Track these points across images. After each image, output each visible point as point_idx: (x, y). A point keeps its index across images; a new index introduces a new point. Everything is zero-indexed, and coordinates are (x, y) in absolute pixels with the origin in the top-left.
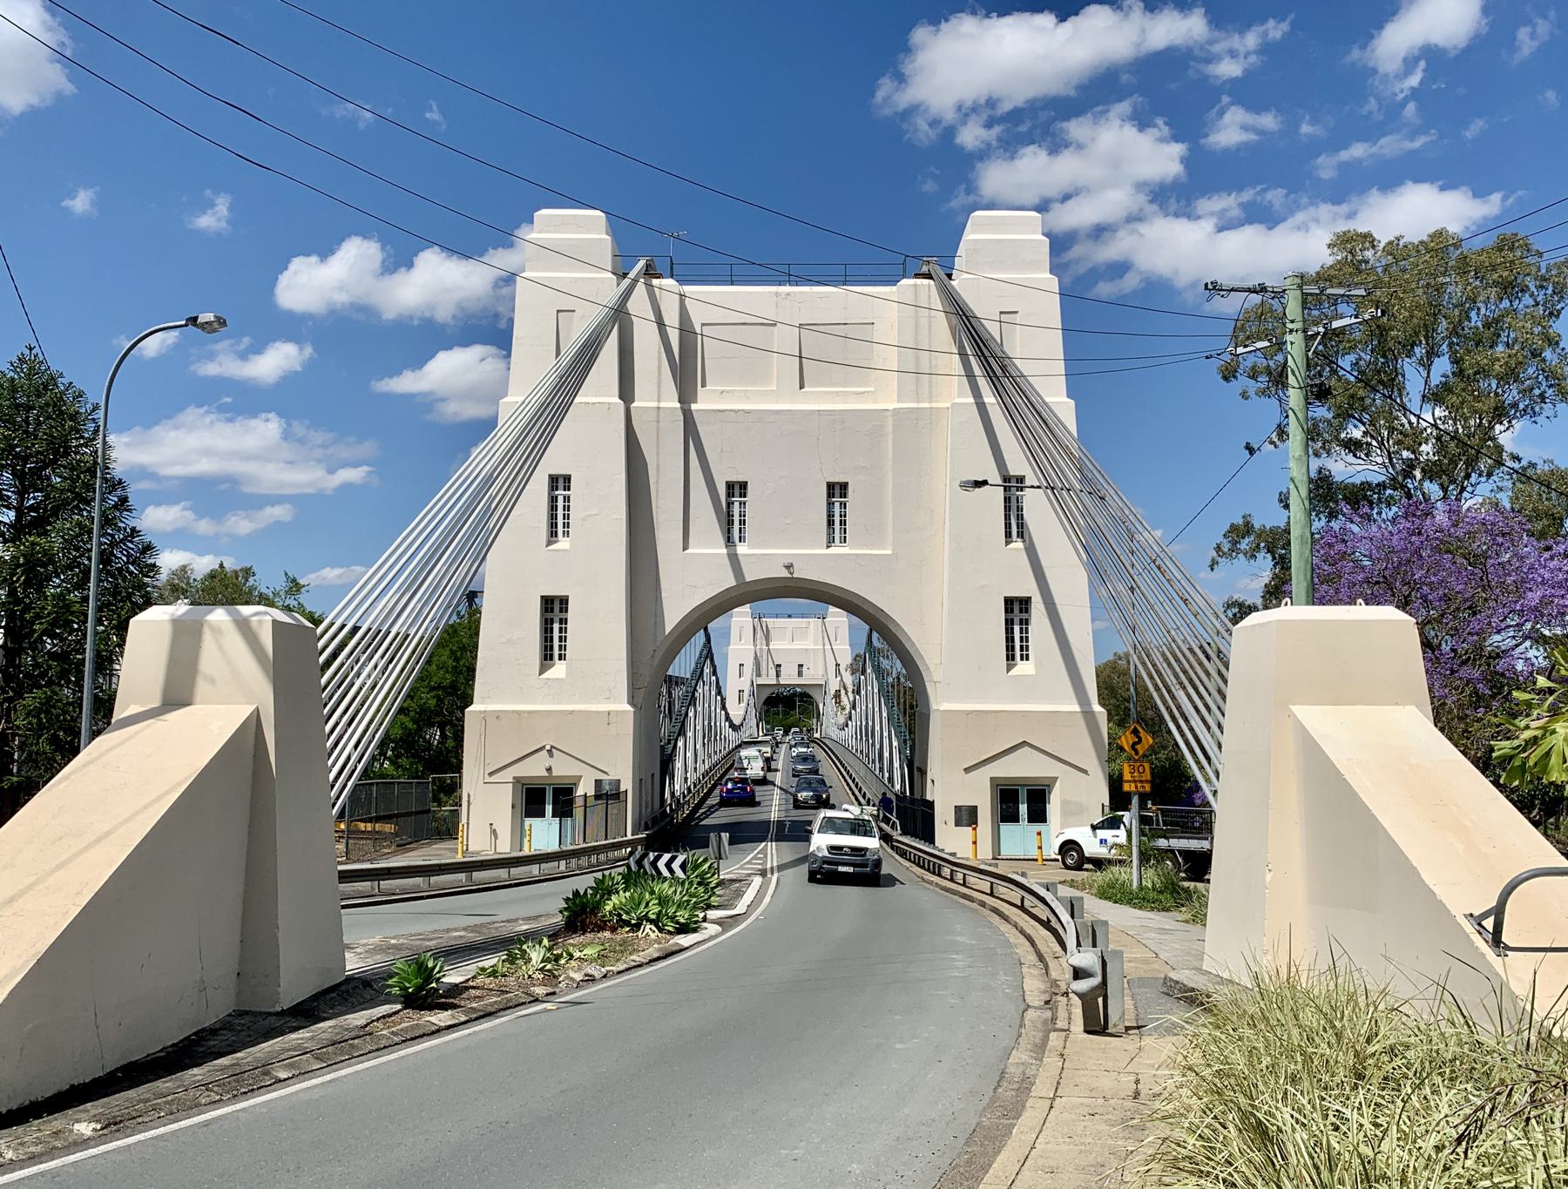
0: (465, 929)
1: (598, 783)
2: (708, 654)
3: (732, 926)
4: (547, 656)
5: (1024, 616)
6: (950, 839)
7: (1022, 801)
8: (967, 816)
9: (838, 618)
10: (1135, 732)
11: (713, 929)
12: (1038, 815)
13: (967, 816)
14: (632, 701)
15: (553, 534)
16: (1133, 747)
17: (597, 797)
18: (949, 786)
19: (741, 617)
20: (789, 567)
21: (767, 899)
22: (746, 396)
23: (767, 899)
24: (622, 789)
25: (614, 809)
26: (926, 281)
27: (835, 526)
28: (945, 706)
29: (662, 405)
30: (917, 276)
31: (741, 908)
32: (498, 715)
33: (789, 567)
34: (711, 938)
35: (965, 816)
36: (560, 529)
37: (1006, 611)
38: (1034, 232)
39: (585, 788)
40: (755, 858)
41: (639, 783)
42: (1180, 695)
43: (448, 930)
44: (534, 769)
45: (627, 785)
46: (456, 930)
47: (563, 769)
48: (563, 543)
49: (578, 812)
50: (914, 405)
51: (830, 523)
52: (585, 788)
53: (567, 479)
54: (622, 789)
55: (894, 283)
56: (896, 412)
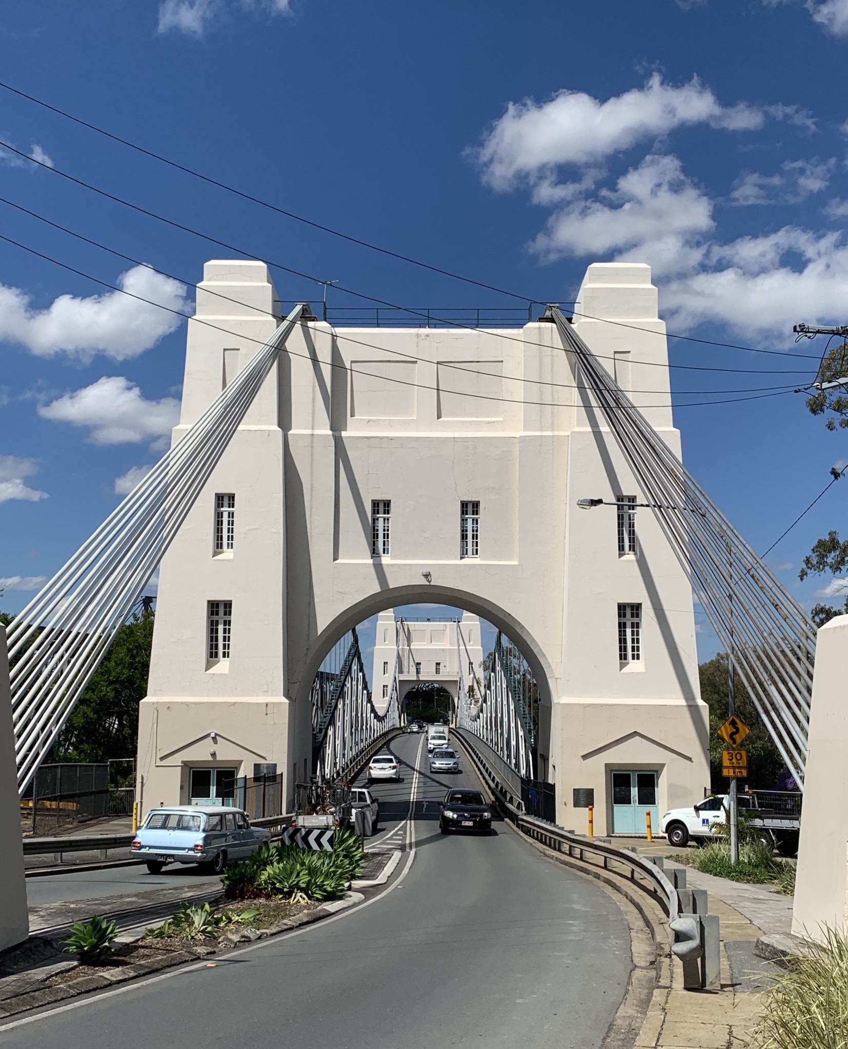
0: (136, 895)
1: (257, 767)
2: (355, 653)
3: (374, 895)
4: (213, 654)
5: (635, 620)
6: (570, 818)
7: (633, 784)
8: (584, 798)
9: (471, 622)
10: (733, 723)
11: (356, 897)
12: (648, 798)
13: (584, 798)
14: (287, 694)
15: (219, 546)
16: (731, 736)
17: (256, 779)
18: (568, 771)
19: (386, 620)
20: (427, 576)
21: (406, 871)
22: (390, 425)
23: (406, 871)
24: (278, 772)
25: (270, 790)
26: (549, 325)
27: (468, 540)
28: (565, 700)
29: (316, 432)
30: (541, 320)
31: (381, 879)
32: (169, 706)
33: (427, 576)
34: (355, 905)
35: (582, 800)
36: (221, 650)
37: (619, 616)
38: (645, 282)
39: (245, 771)
40: (396, 834)
41: (294, 767)
42: (772, 689)
43: (121, 896)
44: (200, 754)
45: (282, 769)
46: (128, 896)
47: (226, 754)
48: (227, 554)
49: (239, 793)
50: (538, 433)
51: (464, 537)
52: (245, 771)
53: (232, 497)
54: (278, 772)
55: (520, 325)
56: (523, 439)
